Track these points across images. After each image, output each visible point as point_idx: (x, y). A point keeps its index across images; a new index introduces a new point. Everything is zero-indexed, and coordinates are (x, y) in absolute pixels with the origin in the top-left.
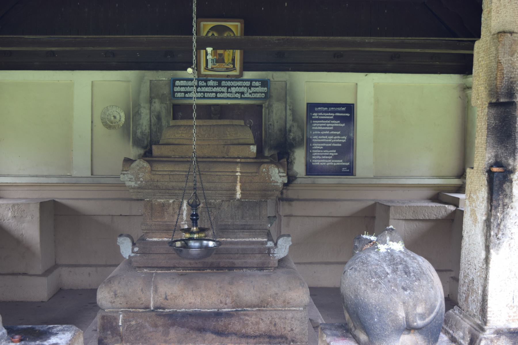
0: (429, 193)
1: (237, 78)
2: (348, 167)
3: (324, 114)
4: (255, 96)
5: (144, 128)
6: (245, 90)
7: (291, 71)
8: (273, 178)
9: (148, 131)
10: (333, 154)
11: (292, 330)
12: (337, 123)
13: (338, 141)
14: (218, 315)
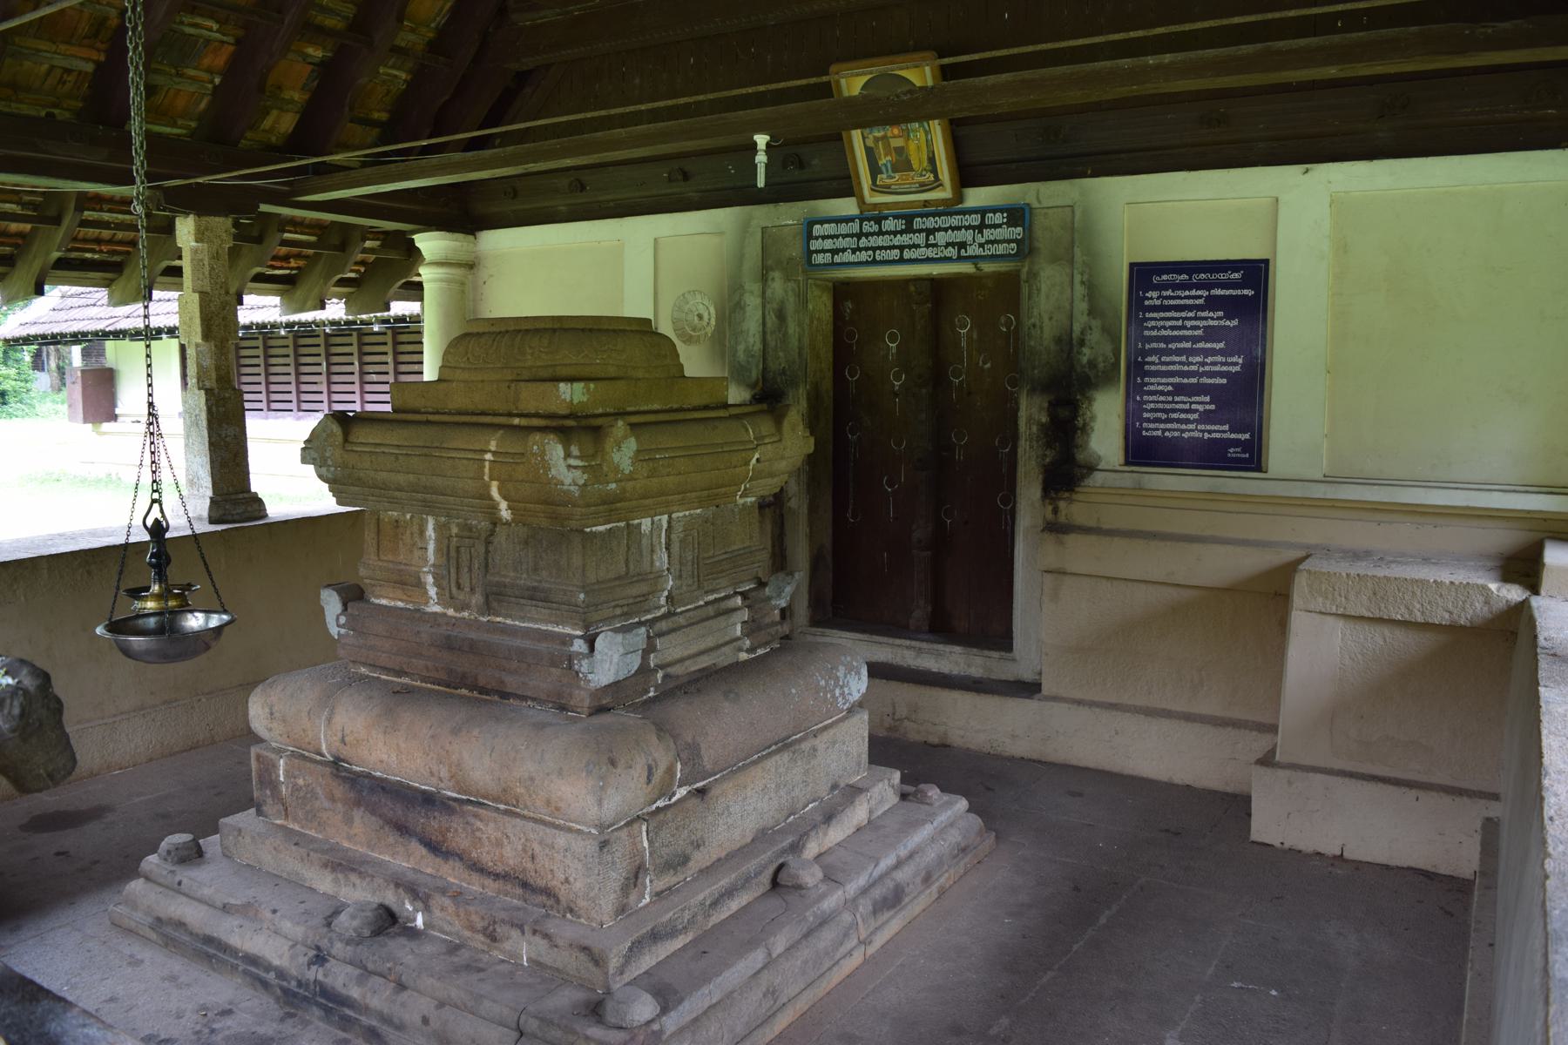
1: (950, 208)
3: (1179, 293)
4: (993, 251)
5: (751, 340)
6: (966, 236)
8: (553, 472)
9: (758, 346)
10: (1200, 408)
11: (567, 881)
12: (1214, 319)
13: (1217, 368)
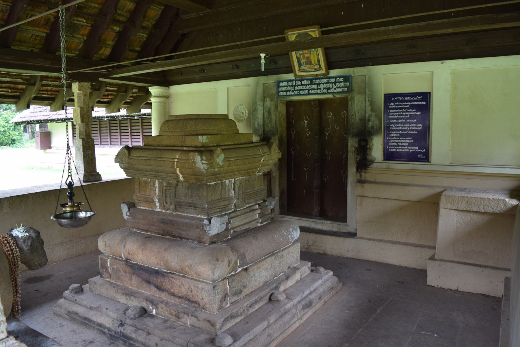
0: (511, 184)
1: (325, 76)
2: (424, 154)
5: (260, 121)
6: (330, 85)
7: (373, 65)
8: (197, 165)
9: (262, 123)
10: (409, 141)
11: (202, 299)
12: (413, 112)
13: (414, 128)
14: (157, 273)
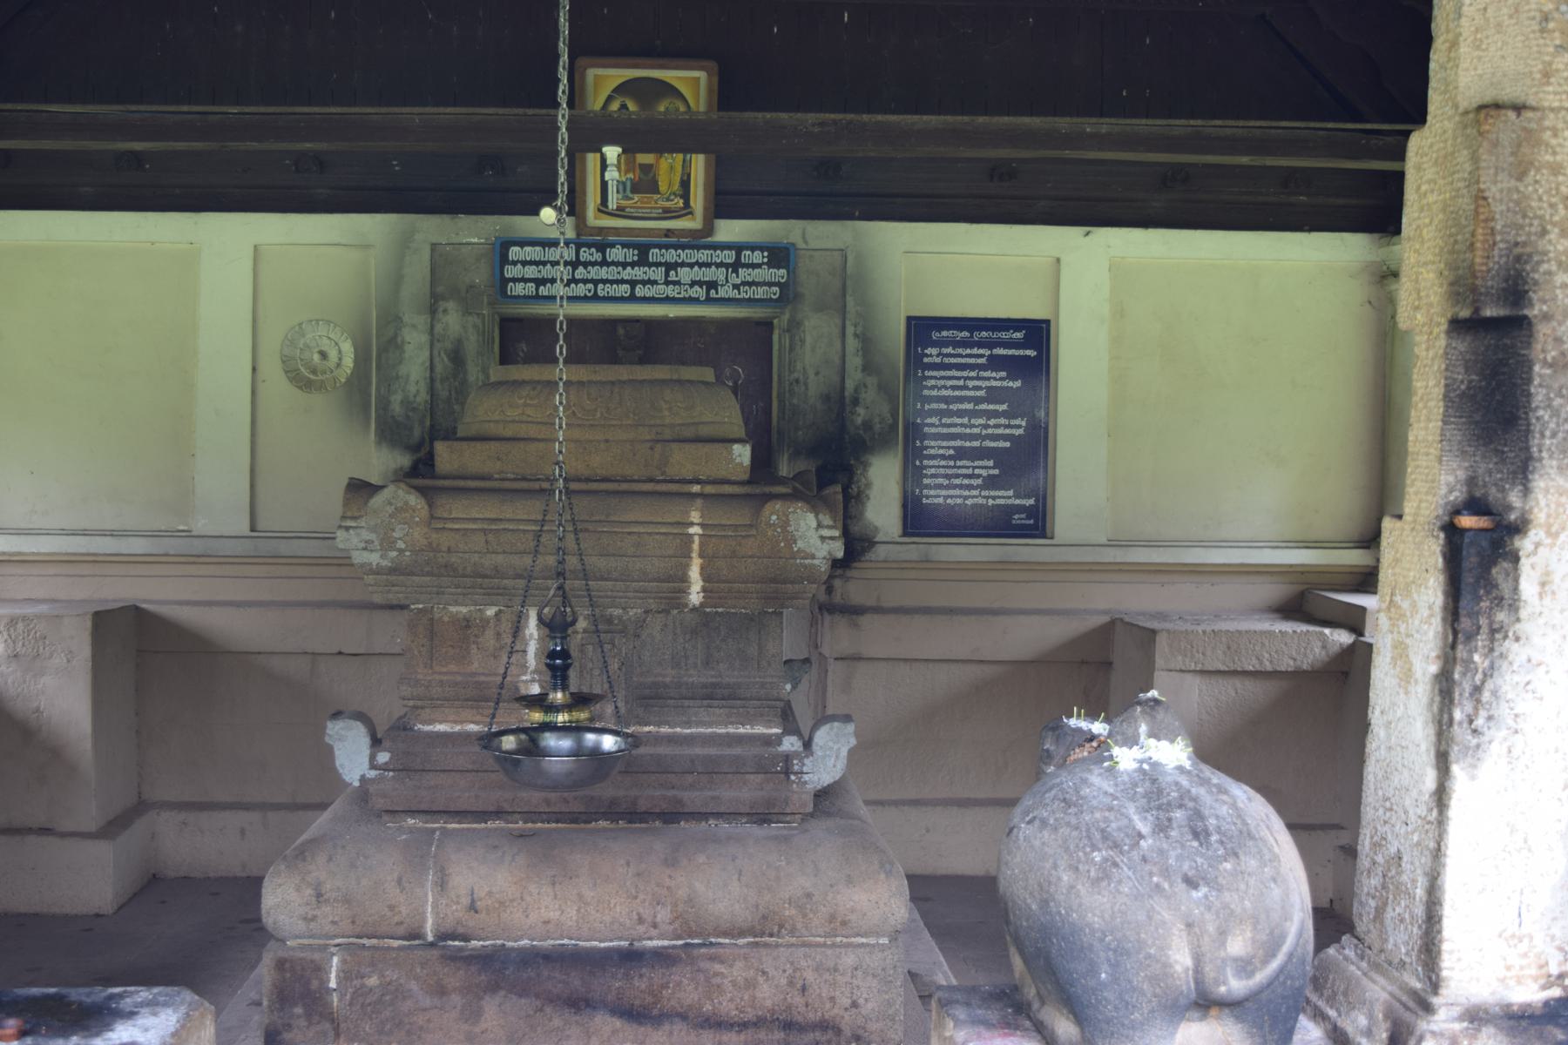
1: (696, 240)
3: (960, 351)
4: (750, 295)
5: (412, 389)
6: (720, 275)
7: (861, 218)
8: (800, 544)
9: (423, 396)
10: (984, 473)
11: (855, 1005)
12: (997, 379)
13: (1000, 431)
14: (631, 958)
